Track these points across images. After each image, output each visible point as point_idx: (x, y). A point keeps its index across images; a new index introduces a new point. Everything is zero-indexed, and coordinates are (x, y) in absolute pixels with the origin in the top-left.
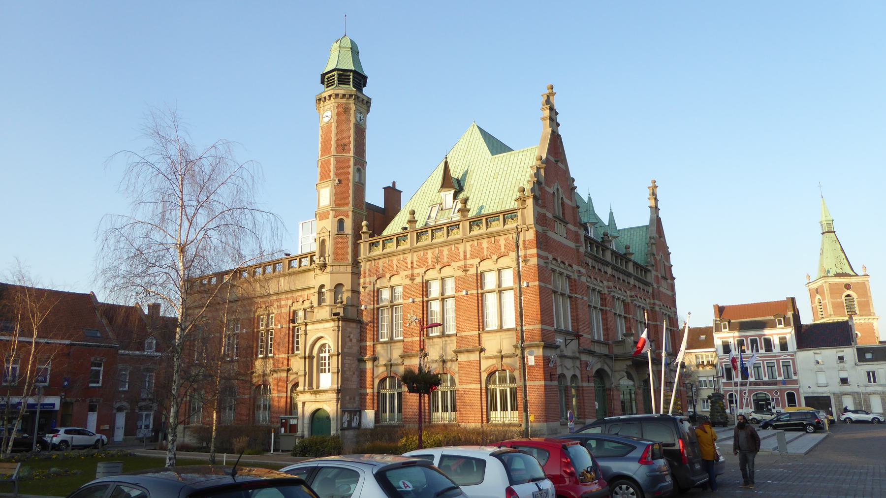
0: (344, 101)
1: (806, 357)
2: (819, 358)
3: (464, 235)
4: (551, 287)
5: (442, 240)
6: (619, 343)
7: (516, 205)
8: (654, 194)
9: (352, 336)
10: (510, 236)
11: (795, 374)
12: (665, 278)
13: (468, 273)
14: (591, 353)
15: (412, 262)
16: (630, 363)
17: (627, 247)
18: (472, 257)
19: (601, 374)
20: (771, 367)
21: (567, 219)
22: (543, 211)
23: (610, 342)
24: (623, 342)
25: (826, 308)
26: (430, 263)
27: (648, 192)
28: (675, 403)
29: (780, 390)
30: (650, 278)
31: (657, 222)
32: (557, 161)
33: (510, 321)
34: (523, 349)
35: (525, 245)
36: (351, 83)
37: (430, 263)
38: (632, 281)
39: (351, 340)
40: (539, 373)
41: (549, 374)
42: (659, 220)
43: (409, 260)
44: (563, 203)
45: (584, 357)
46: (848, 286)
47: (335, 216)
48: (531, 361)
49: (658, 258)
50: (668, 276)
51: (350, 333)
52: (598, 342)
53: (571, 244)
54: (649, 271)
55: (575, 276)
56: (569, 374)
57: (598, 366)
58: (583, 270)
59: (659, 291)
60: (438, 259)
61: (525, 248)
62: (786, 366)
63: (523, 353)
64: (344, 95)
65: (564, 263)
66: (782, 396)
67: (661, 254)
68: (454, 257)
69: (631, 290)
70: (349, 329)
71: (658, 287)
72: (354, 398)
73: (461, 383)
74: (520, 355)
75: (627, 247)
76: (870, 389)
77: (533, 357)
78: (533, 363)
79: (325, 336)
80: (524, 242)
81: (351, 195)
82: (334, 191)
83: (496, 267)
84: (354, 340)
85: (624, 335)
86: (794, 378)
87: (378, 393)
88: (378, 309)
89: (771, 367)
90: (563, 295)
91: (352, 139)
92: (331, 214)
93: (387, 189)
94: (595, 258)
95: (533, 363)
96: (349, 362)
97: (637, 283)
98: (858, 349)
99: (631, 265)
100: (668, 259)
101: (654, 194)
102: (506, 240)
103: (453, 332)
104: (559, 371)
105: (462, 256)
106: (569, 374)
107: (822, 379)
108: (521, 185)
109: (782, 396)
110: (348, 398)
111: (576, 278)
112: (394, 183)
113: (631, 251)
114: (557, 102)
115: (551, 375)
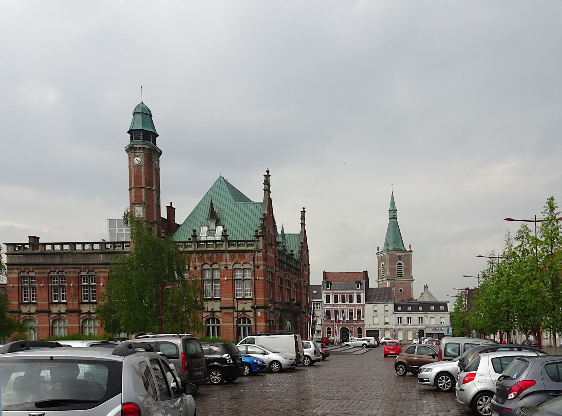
1: (369, 309)
2: (376, 308)
3: (226, 248)
7: (253, 238)
11: (363, 317)
12: (306, 265)
20: (351, 314)
25: (386, 271)
28: (43, 304)
29: (355, 326)
31: (304, 233)
40: (263, 320)
41: (267, 321)
46: (400, 257)
48: (259, 314)
61: (258, 261)
62: (359, 312)
66: (355, 329)
73: (223, 322)
76: (398, 327)
81: (155, 213)
83: (242, 268)
86: (362, 319)
89: (351, 314)
98: (395, 304)
99: (293, 261)
105: (224, 259)
107: (376, 320)
109: (355, 329)
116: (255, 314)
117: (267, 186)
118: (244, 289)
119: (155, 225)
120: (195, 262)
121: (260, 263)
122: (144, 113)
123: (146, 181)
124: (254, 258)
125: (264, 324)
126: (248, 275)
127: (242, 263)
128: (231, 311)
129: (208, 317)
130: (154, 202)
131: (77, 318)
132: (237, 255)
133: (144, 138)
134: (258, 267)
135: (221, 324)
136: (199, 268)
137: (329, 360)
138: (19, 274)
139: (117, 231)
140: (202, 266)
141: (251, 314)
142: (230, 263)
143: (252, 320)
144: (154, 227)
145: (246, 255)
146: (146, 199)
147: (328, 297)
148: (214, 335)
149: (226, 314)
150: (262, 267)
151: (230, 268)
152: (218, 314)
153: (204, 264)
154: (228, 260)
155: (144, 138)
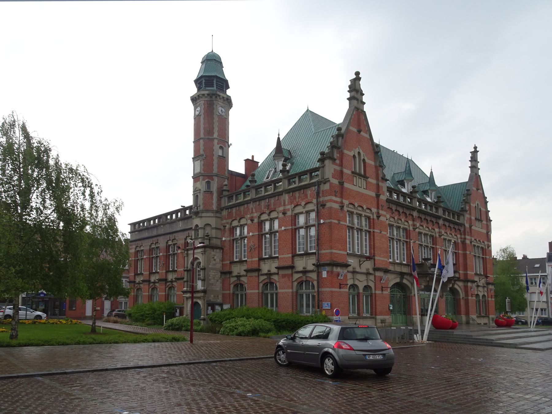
4: (348, 224)
5: (272, 192)
7: (318, 165)
9: (215, 257)
13: (287, 215)
19: (400, 286)
21: (368, 175)
30: (465, 220)
32: (359, 131)
35: (323, 194)
45: (378, 274)
48: (324, 274)
56: (481, 294)
60: (268, 206)
64: (208, 95)
71: (470, 227)
72: (218, 296)
73: (280, 289)
78: (326, 276)
82: (202, 162)
83: (304, 211)
84: (218, 260)
85: (423, 259)
88: (233, 240)
90: (360, 230)
93: (247, 161)
95: (326, 276)
96: (213, 274)
106: (481, 294)
108: (322, 151)
112: (253, 157)
113: (441, 200)
114: (363, 85)
115: (340, 284)
116: (319, 274)
117: (474, 163)
120: (252, 213)
122: (212, 61)
127: (303, 203)
128: (289, 272)
129: (265, 281)
131: (164, 287)
132: (297, 194)
136: (256, 220)
138: (136, 249)
140: (259, 217)
141: (314, 276)
142: (289, 207)
144: (213, 180)
145: (309, 192)
146: (204, 151)
148: (272, 305)
149: (284, 276)
151: (289, 213)
152: (275, 277)
153: (260, 215)
154: (287, 203)
155: (212, 87)
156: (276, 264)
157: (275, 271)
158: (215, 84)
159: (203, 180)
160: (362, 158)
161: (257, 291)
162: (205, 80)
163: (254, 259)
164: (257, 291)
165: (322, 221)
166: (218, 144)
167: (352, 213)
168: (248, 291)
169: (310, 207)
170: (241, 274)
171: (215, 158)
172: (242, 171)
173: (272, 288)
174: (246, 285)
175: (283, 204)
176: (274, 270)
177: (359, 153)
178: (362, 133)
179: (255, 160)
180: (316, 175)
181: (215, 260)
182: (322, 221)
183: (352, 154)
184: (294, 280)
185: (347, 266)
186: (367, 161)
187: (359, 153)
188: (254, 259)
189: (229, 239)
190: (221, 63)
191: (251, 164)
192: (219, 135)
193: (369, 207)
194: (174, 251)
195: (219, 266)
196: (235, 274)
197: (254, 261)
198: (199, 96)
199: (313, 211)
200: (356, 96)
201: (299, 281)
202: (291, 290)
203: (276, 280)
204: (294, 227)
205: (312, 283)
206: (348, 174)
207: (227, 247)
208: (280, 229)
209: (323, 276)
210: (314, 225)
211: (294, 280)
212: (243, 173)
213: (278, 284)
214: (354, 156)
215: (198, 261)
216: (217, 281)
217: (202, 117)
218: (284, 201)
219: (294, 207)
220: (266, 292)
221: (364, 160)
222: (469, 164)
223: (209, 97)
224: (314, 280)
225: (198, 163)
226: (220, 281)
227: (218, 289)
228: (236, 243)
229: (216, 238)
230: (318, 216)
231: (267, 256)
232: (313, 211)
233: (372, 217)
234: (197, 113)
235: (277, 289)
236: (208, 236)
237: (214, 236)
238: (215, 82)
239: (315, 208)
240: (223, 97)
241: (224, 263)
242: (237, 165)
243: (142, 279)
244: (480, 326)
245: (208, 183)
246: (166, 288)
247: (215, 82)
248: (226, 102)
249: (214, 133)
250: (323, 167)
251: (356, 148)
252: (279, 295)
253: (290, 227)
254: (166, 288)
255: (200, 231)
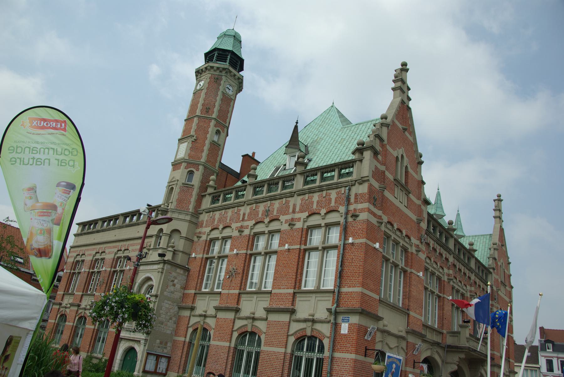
0: (217, 73)
6: (455, 334)
7: (352, 157)
8: (498, 209)
9: (176, 281)
10: (343, 189)
14: (422, 337)
15: (244, 214)
16: (463, 356)
17: (471, 244)
18: (301, 211)
22: (382, 168)
23: (445, 332)
24: (458, 333)
26: (260, 216)
27: (493, 205)
32: (405, 130)
33: (329, 283)
34: (336, 314)
36: (228, 61)
37: (260, 216)
38: (473, 277)
39: (174, 285)
42: (502, 230)
43: (242, 213)
44: (407, 172)
47: (186, 168)
48: (344, 329)
49: (499, 264)
50: (507, 284)
51: (176, 278)
52: (432, 329)
53: (414, 217)
54: (491, 273)
55: (413, 250)
57: (427, 354)
58: (423, 248)
59: (498, 295)
60: (267, 212)
63: (335, 319)
65: (401, 231)
67: (501, 261)
68: (284, 210)
69: (471, 286)
70: (174, 274)
72: (166, 343)
73: (267, 344)
74: (332, 321)
75: (471, 244)
77: (347, 325)
78: (346, 332)
79: (152, 277)
80: (356, 195)
82: (190, 145)
84: (178, 286)
85: (461, 326)
87: (235, 348)
91: (217, 104)
92: (184, 165)
93: (245, 157)
94: (438, 242)
95: (346, 332)
96: (167, 306)
97: (478, 281)
100: (508, 269)
101: (498, 209)
102: (338, 193)
103: (269, 289)
104: (378, 347)
110: (158, 341)
111: (414, 252)
112: (254, 154)
113: (475, 247)
115: (366, 349)
116: (336, 327)
118: (322, 272)
119: (201, 167)
121: (360, 206)
123: (212, 112)
124: (348, 199)
125: (353, 356)
126: (335, 236)
130: (208, 136)
133: (225, 62)
134: (355, 216)
135: (263, 348)
137: (438, 194)
139: (310, 355)
141: (325, 330)
143: (326, 342)
147: (550, 363)
150: (363, 216)
154: (297, 210)
155: (225, 62)
156: (265, 303)
157: (263, 314)
158: (228, 59)
159: (186, 168)
160: (405, 165)
161: (227, 344)
162: (219, 54)
163: (232, 292)
164: (227, 344)
165: (350, 240)
166: (215, 126)
167: (388, 237)
168: (212, 342)
169: (333, 218)
170: (209, 313)
171: (207, 142)
172: (237, 168)
173: (251, 343)
174: (212, 332)
175: (291, 210)
176: (260, 313)
177: (402, 156)
178: (406, 133)
179: (256, 158)
180: (347, 173)
181: (174, 285)
182: (350, 240)
183: (395, 154)
184: (290, 333)
185: (379, 319)
186: (410, 170)
187: (402, 156)
188: (232, 292)
189: (201, 256)
190: (241, 42)
191: (249, 161)
192: (219, 116)
193: (409, 235)
194: (122, 267)
195: (178, 295)
196: (199, 311)
197: (232, 294)
198: (206, 68)
199: (337, 224)
200: (402, 87)
201: (299, 335)
202: (283, 350)
203: (260, 330)
204: (303, 247)
205: (259, 337)
206: (390, 180)
207: (194, 268)
208: (282, 248)
209: (342, 332)
210: (335, 247)
211: (290, 333)
212: (238, 171)
213: (263, 337)
214: (397, 157)
215: (150, 283)
216: (171, 319)
217: (203, 95)
218: (295, 206)
219: (308, 217)
220: (298, 354)
221: (406, 167)
222: (493, 213)
223: (218, 71)
224: (324, 337)
225: (184, 146)
226: (174, 319)
227: (169, 332)
228: (211, 265)
229: (183, 252)
230: (345, 232)
231: (253, 289)
232: (337, 224)
233: (409, 250)
234: (198, 88)
235: (259, 345)
236: (173, 247)
237: (181, 249)
238: (229, 57)
239: (342, 220)
240: (235, 75)
241: (186, 292)
242: (232, 160)
243: (71, 301)
244: (145, 330)
245: (191, 173)
246: (76, 316)
247: (229, 57)
248: (236, 82)
249: (213, 112)
250: (361, 161)
251: (399, 149)
252: (262, 356)
253: (298, 247)
254: (76, 316)
255: (163, 237)
